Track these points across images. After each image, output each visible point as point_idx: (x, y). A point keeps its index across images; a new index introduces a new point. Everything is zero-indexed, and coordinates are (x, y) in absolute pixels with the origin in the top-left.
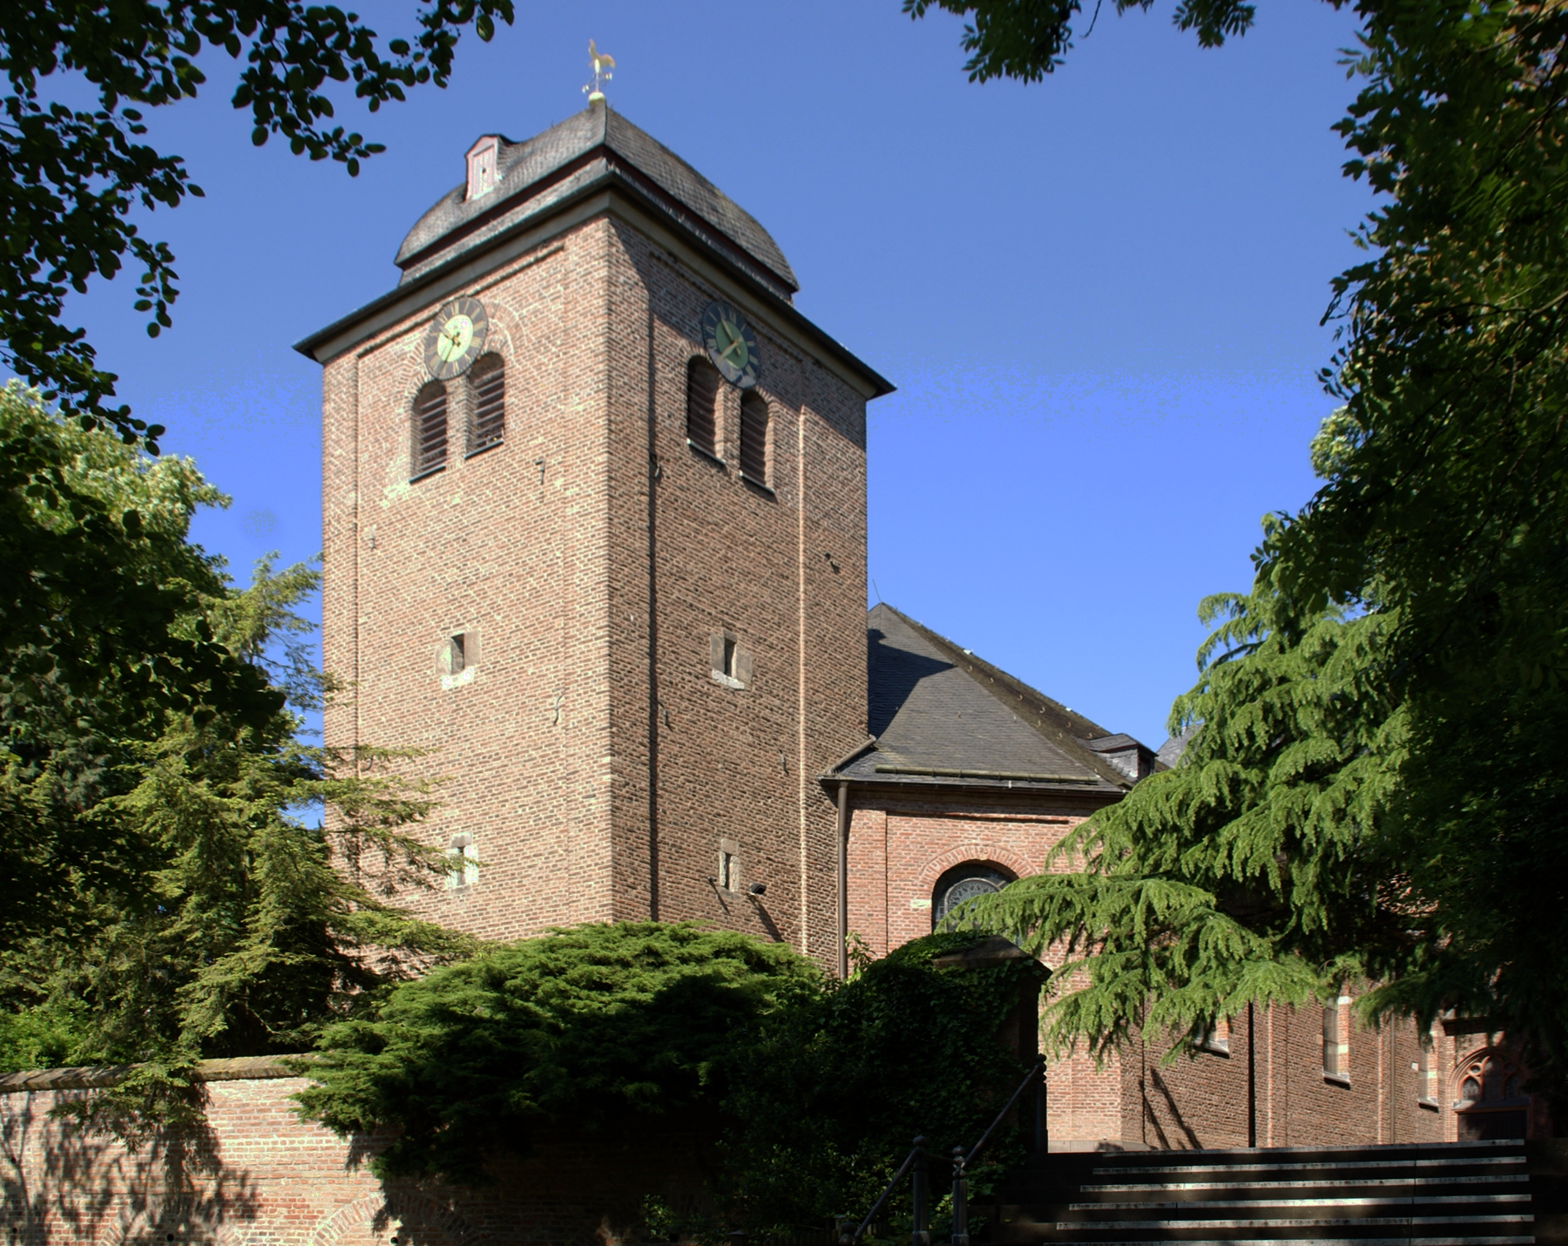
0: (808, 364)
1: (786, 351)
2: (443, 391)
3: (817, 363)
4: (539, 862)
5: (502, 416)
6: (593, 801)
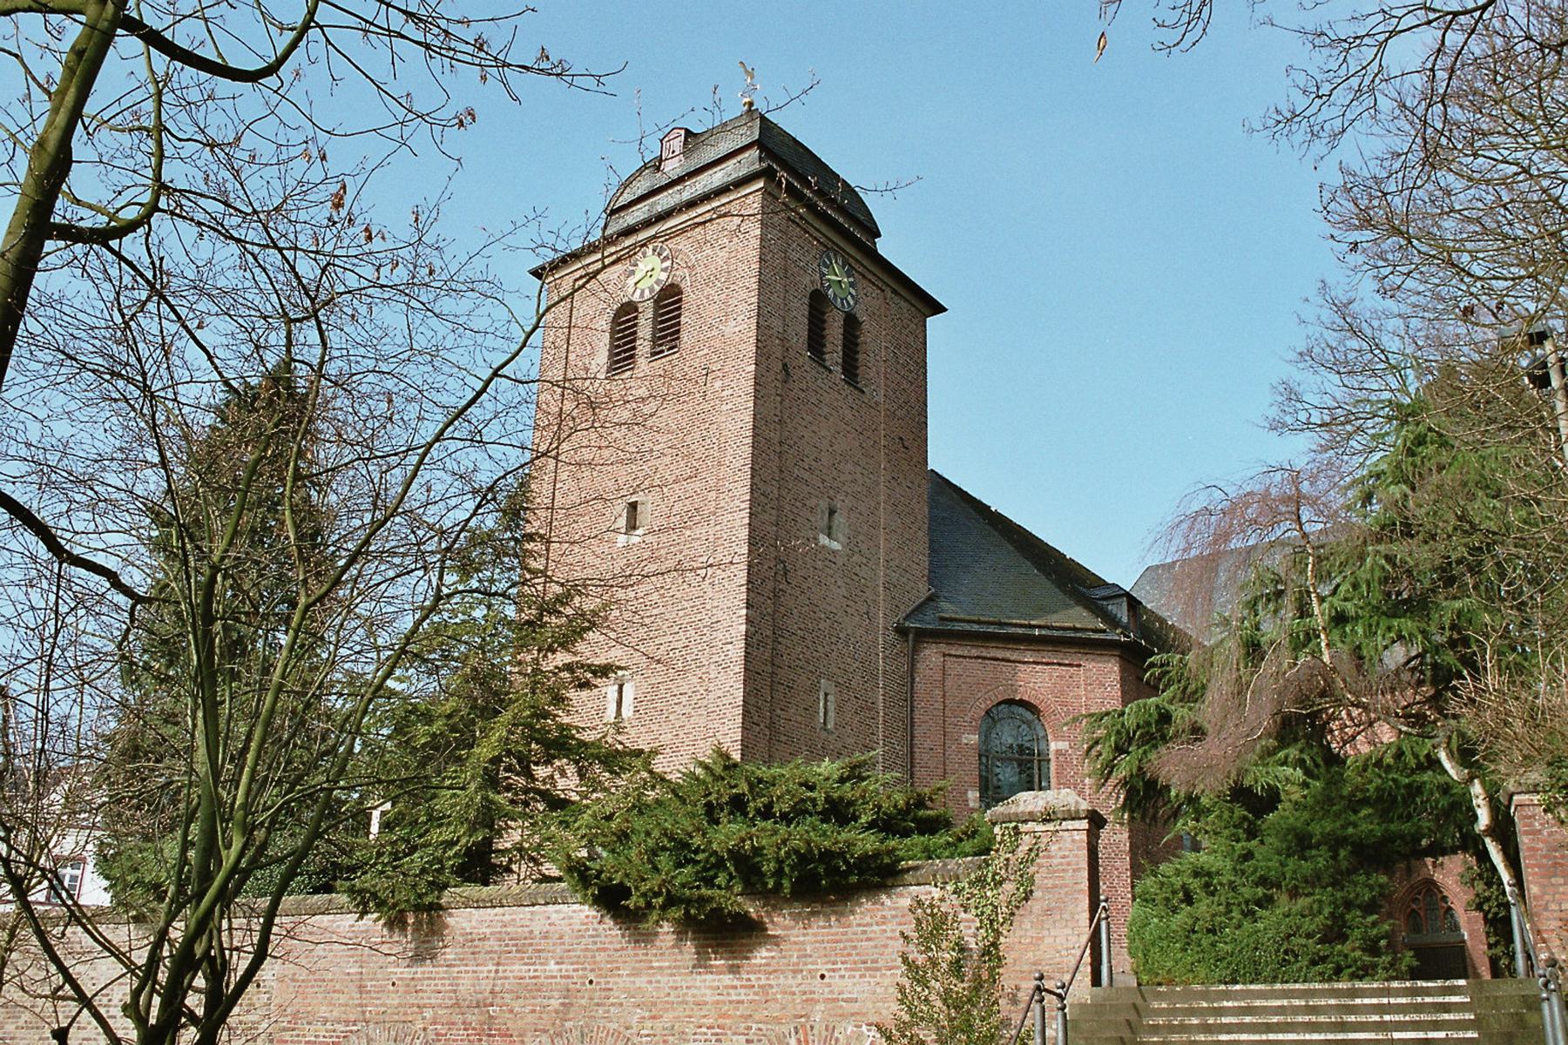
0: (889, 294)
1: (874, 284)
2: (636, 310)
3: (894, 292)
4: (684, 699)
5: (678, 331)
6: (730, 646)
